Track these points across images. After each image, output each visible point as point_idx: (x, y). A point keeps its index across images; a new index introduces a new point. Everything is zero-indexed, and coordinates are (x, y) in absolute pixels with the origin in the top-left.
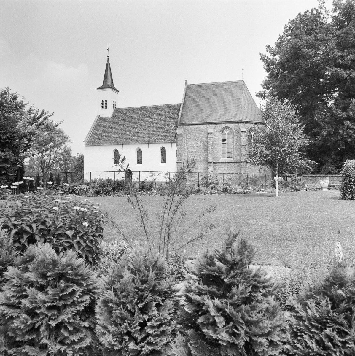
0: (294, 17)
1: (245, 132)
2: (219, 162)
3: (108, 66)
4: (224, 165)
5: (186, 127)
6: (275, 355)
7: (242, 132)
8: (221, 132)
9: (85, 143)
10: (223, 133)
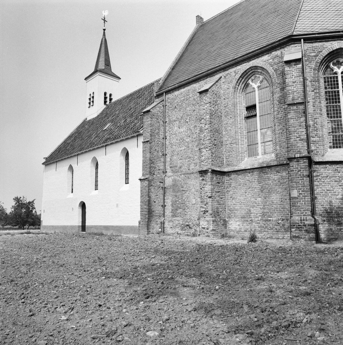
2: (236, 168)
3: (104, 43)
4: (249, 176)
5: (170, 96)
6: (342, 73)
9: (44, 160)
10: (249, 90)
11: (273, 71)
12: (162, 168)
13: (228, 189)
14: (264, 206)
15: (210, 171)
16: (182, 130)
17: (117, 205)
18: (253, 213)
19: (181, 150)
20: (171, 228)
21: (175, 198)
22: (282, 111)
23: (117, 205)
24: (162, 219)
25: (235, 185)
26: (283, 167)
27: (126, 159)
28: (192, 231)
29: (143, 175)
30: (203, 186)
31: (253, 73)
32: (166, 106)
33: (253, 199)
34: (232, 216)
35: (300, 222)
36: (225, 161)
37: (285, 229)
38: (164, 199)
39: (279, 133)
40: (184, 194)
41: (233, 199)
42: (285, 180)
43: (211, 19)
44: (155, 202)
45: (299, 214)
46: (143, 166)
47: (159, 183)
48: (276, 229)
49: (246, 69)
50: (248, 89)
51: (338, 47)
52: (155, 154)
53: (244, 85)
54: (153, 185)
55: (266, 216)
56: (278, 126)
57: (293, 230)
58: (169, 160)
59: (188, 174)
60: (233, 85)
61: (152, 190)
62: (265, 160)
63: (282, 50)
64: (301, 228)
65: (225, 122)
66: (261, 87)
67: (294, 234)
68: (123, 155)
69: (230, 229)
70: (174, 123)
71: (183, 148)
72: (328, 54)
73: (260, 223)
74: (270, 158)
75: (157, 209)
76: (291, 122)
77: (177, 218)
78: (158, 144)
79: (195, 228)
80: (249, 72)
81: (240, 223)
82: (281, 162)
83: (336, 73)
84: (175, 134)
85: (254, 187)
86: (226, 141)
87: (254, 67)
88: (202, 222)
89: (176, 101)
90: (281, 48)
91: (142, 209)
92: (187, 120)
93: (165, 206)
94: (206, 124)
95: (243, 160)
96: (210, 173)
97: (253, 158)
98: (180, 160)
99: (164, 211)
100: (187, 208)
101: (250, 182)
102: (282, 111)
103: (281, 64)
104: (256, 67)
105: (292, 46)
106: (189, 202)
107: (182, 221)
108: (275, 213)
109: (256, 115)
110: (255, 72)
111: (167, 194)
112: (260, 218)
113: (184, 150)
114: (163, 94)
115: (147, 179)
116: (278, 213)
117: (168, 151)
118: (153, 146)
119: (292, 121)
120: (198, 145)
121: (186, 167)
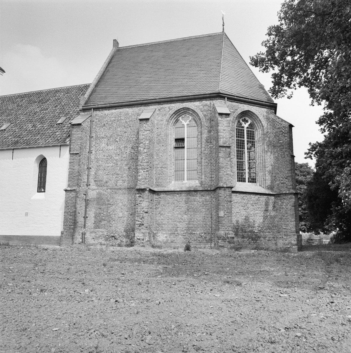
0: (263, 85)
1: (227, 115)
2: (166, 189)
4: (177, 197)
7: (221, 114)
8: (173, 120)
10: (178, 125)
11: (203, 116)
12: (86, 180)
13: (156, 206)
14: (189, 222)
15: (148, 190)
16: (111, 148)
17: (27, 214)
18: (179, 227)
19: (108, 167)
20: (93, 238)
21: (99, 210)
22: (208, 149)
23: (27, 214)
24: (83, 230)
25: (164, 203)
26: (207, 193)
27: (39, 167)
28: (118, 242)
29: (68, 186)
30: (140, 203)
31: (185, 113)
32: (93, 121)
33: (180, 216)
34: (159, 229)
35: (224, 235)
36: (154, 182)
37: (206, 241)
38: (86, 211)
39: (205, 166)
40: (109, 207)
41: (161, 215)
42: (208, 203)
43: (129, 47)
44: (79, 213)
45: (224, 229)
46: (69, 177)
47: (83, 195)
48: (199, 241)
49: (180, 108)
50: (178, 124)
51: (247, 110)
52: (82, 166)
53: (175, 120)
54: (79, 196)
55: (190, 230)
56: (204, 159)
57: (220, 241)
58: (94, 174)
59: (115, 189)
60: (166, 118)
61: (78, 202)
62: (191, 185)
63: (211, 101)
64: (225, 239)
65: (157, 148)
66: (190, 125)
67: (220, 244)
68: (37, 162)
69: (157, 240)
70: (102, 139)
71: (111, 165)
72: (241, 113)
73: (185, 236)
74: (195, 184)
75: (80, 220)
76: (221, 160)
77: (100, 230)
78: (84, 157)
79: (121, 239)
80: (181, 111)
81: (167, 235)
82: (206, 188)
83: (243, 127)
84: (102, 150)
85: (181, 206)
86: (157, 164)
87: (187, 108)
88: (138, 234)
89: (105, 120)
90: (210, 100)
91: (66, 219)
92: (117, 140)
93: (87, 217)
94: (145, 148)
95: (171, 183)
96: (148, 191)
97: (180, 182)
98: (106, 175)
99: (85, 222)
100: (112, 220)
101: (179, 202)
102: (208, 149)
103: (210, 112)
104: (188, 109)
105: (219, 100)
106: (115, 215)
107: (107, 232)
108: (199, 227)
109: (184, 147)
110: (186, 112)
111: (90, 206)
112: (185, 231)
113: (112, 166)
114: (91, 109)
115: (74, 190)
116: (201, 228)
117: (93, 165)
118: (81, 159)
119: (221, 159)
120: (127, 164)
121: (113, 183)
